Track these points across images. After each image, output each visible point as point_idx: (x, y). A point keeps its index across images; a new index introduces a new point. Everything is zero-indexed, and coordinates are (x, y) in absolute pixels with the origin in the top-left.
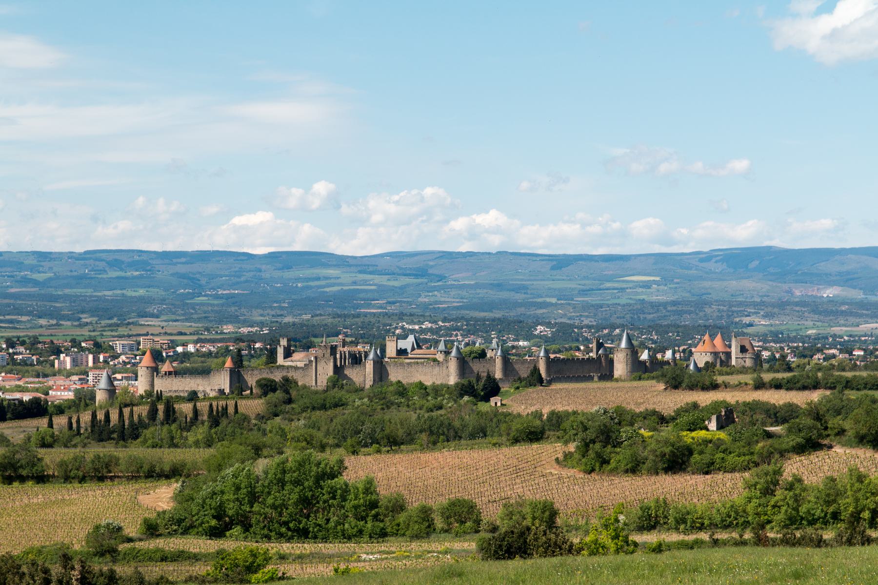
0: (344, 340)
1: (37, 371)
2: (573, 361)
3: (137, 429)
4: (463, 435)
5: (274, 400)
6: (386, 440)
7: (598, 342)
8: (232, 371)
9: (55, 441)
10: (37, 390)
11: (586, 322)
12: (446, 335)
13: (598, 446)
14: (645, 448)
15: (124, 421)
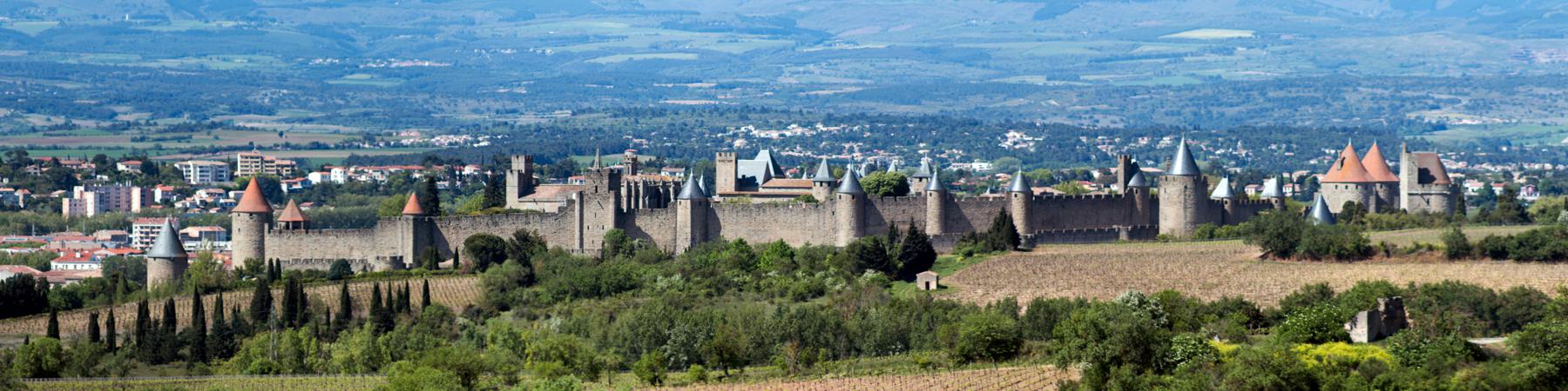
0: (635, 160)
1: (25, 221)
2: (1079, 200)
3: (230, 336)
4: (864, 347)
5: (500, 277)
6: (715, 357)
7: (1127, 162)
8: (418, 221)
9: (62, 364)
10: (25, 260)
11: (1104, 123)
12: (831, 151)
13: (1126, 370)
14: (1221, 375)
15: (203, 322)
